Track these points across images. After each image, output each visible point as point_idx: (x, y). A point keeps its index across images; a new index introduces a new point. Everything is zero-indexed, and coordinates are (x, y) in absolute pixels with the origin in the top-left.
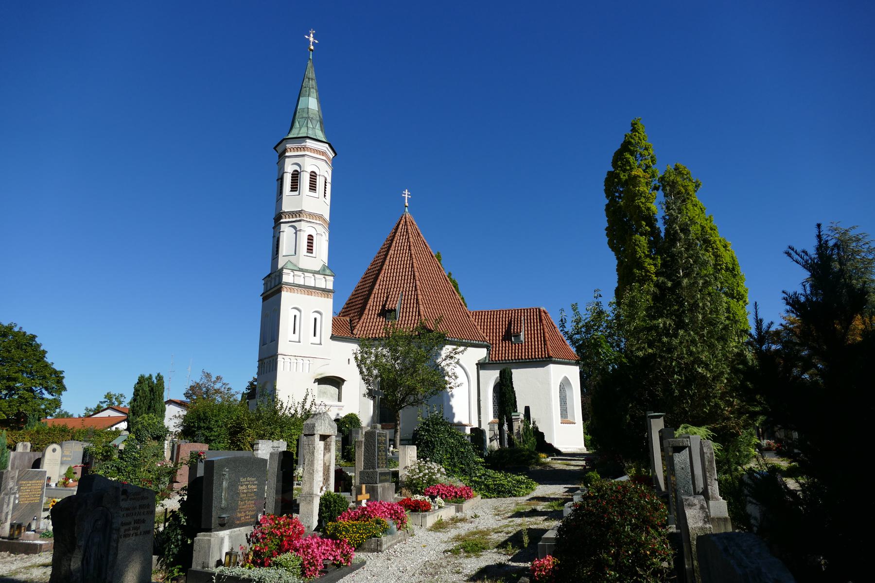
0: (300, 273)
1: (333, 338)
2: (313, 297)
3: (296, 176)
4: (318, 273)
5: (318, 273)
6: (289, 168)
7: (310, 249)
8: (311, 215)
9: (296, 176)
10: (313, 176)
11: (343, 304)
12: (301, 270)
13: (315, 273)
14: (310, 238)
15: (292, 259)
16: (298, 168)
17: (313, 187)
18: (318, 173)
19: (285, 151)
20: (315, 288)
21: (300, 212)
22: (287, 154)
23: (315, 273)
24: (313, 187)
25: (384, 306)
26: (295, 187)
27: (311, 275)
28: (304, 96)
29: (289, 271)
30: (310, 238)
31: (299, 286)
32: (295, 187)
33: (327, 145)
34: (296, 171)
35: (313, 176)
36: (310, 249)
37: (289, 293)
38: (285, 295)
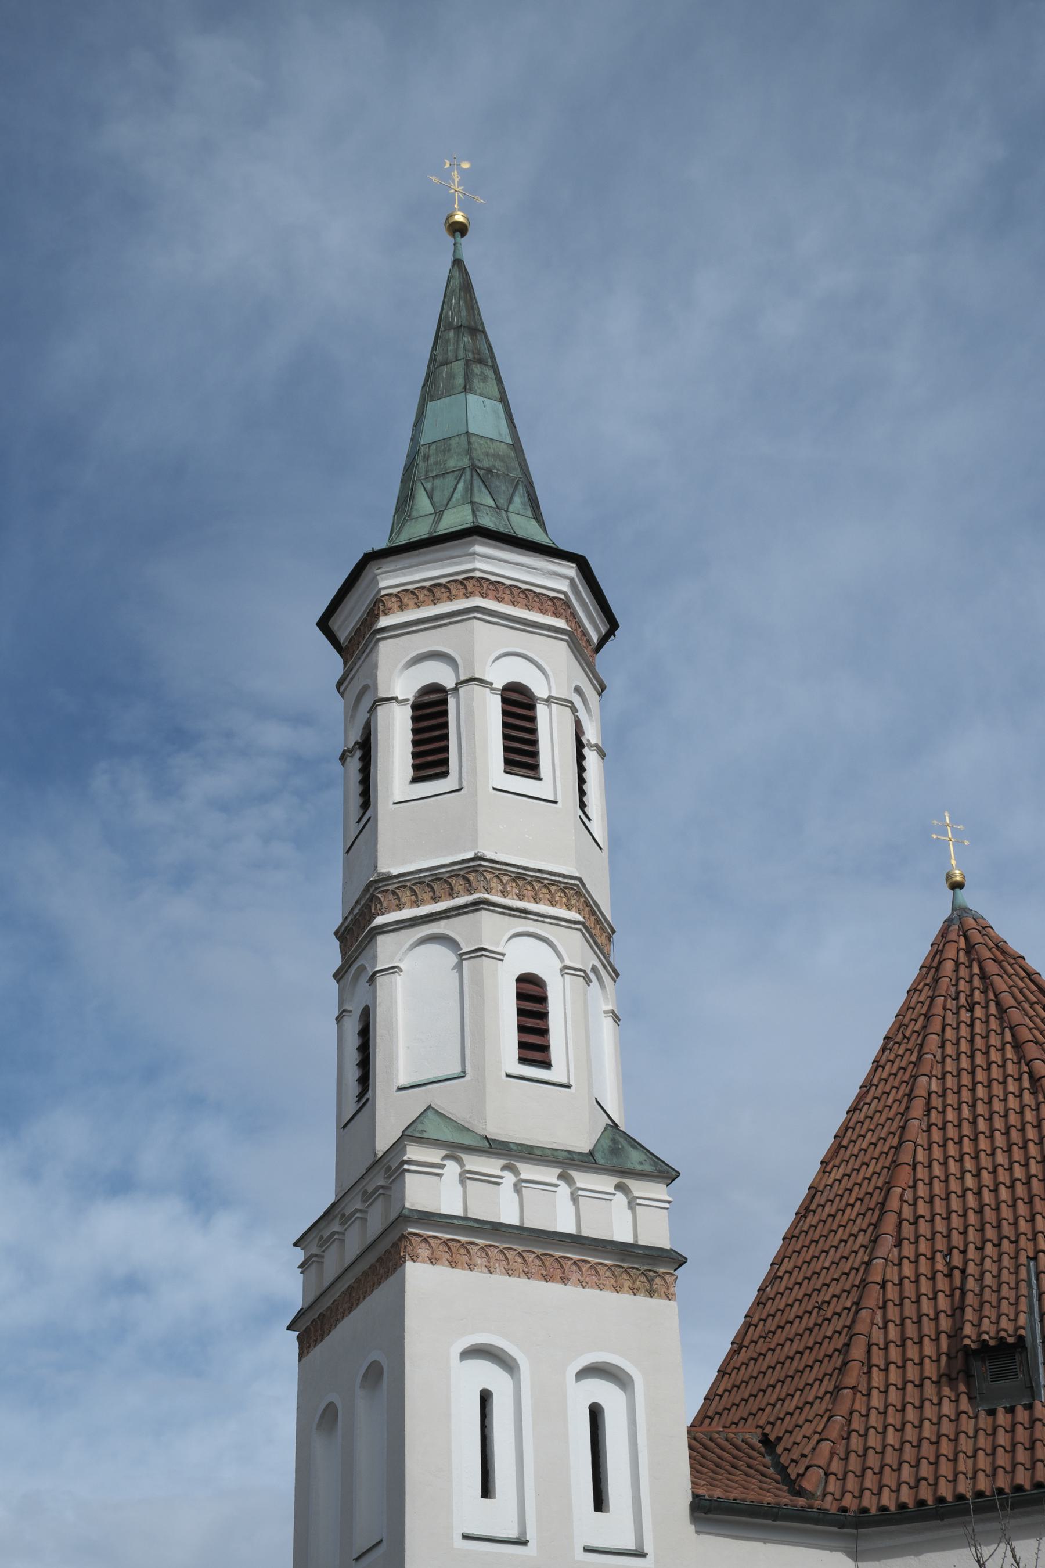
0: (491, 1166)
1: (707, 1511)
2: (478, 1278)
3: (431, 713)
4: (587, 1161)
5: (587, 1161)
6: (399, 676)
7: (534, 1047)
8: (527, 880)
9: (431, 713)
10: (518, 705)
11: (398, 1271)
12: (494, 1147)
13: (568, 1162)
14: (531, 995)
15: (441, 1098)
16: (442, 675)
17: (521, 754)
18: (539, 689)
19: (377, 607)
20: (576, 1241)
21: (474, 871)
22: (384, 622)
23: (568, 1162)
24: (521, 754)
25: (956, 1334)
26: (431, 757)
27: (549, 1174)
28: (449, 392)
29: (434, 1155)
30: (531, 995)
31: (496, 1229)
32: (431, 757)
33: (570, 570)
34: (435, 689)
35: (518, 705)
36: (534, 1047)
37: (442, 1271)
38: (426, 1283)
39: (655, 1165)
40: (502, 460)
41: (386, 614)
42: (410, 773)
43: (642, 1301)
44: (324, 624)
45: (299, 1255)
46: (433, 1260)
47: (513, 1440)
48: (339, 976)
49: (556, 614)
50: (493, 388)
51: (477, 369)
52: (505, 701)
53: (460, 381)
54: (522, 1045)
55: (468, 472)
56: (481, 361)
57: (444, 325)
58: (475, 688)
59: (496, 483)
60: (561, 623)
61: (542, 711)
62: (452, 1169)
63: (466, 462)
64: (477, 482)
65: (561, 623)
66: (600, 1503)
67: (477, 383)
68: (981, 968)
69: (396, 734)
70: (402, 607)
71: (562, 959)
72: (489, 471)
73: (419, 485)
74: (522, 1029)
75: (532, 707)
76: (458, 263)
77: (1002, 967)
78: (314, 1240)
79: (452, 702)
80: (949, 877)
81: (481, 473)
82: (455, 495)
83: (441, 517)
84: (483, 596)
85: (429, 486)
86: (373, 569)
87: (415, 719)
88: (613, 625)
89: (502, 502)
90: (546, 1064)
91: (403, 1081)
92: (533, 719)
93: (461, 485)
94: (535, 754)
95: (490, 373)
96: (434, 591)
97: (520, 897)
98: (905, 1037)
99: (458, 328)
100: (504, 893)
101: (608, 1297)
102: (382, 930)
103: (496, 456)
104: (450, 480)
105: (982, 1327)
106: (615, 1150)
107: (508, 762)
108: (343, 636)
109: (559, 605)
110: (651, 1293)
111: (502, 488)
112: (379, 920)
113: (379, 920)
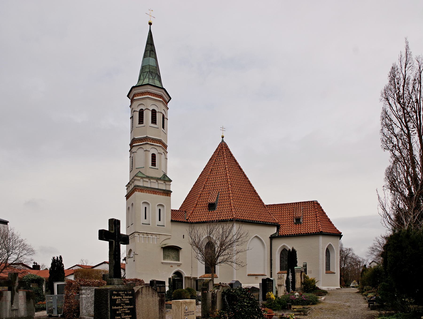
7: (154, 164)
10: (154, 112)
12: (148, 177)
13: (158, 179)
14: (154, 156)
15: (141, 170)
17: (154, 121)
20: (158, 189)
24: (154, 121)
30: (154, 156)
34: (142, 109)
35: (154, 112)
36: (154, 164)
42: (138, 123)
43: (166, 197)
44: (128, 96)
45: (126, 188)
46: (139, 191)
48: (130, 151)
49: (160, 98)
50: (154, 56)
51: (152, 52)
53: (149, 55)
54: (152, 163)
56: (152, 51)
57: (147, 43)
58: (147, 110)
60: (161, 100)
62: (141, 180)
64: (150, 74)
65: (161, 100)
66: (160, 220)
67: (151, 55)
70: (138, 96)
74: (152, 161)
75: (156, 113)
76: (150, 31)
78: (128, 186)
84: (149, 95)
86: (133, 90)
88: (171, 98)
89: (154, 78)
90: (155, 166)
91: (137, 167)
92: (156, 115)
94: (156, 121)
95: (153, 53)
96: (142, 94)
97: (153, 142)
100: (150, 142)
101: (162, 196)
102: (134, 146)
103: (153, 69)
104: (146, 73)
106: (164, 178)
109: (161, 96)
110: (167, 196)
111: (154, 75)
112: (134, 145)
113: (134, 145)
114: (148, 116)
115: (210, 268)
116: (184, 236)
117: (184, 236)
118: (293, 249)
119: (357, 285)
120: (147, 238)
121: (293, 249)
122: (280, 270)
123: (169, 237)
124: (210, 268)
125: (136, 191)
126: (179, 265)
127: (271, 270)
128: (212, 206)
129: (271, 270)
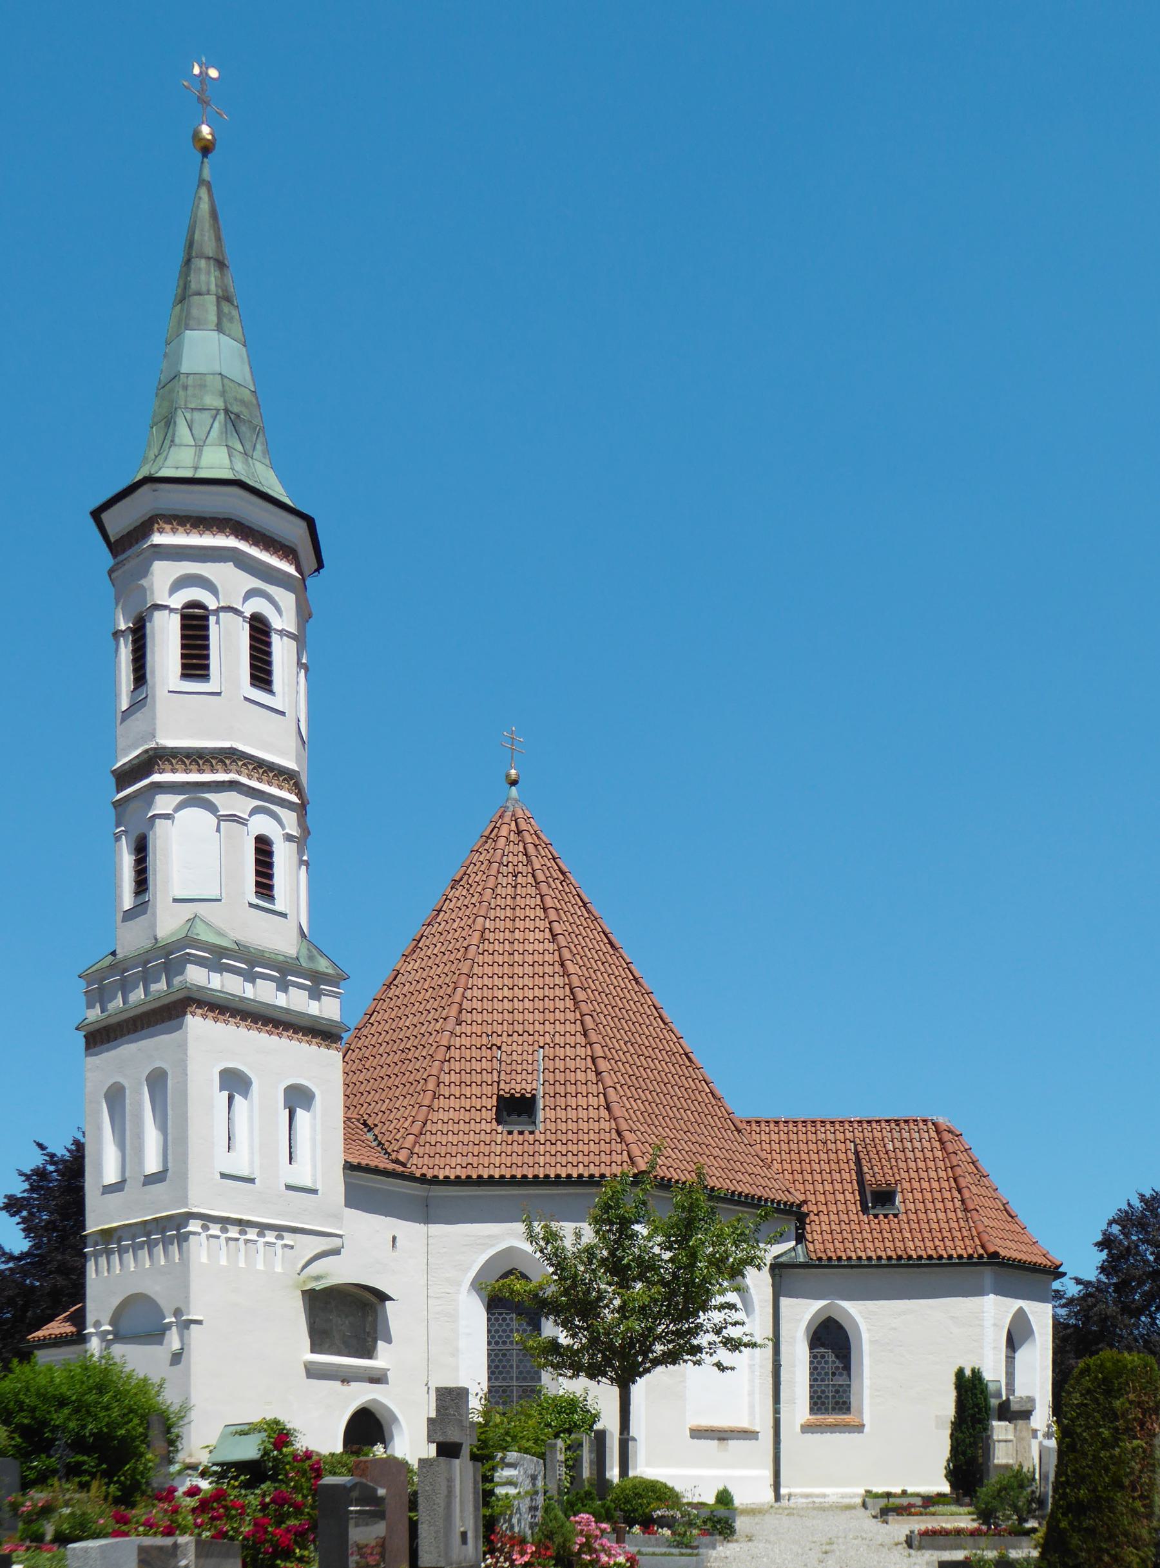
3: (195, 627)
10: (260, 630)
22: (158, 539)
26: (195, 663)
32: (195, 663)
33: (303, 524)
39: (334, 969)
40: (247, 407)
41: (161, 533)
46: (204, 1016)
47: (770, 1380)
51: (226, 308)
52: (252, 627)
53: (213, 318)
55: (222, 413)
59: (243, 429)
61: (275, 639)
63: (219, 403)
67: (226, 324)
68: (525, 848)
69: (167, 637)
71: (283, 827)
72: (238, 416)
73: (179, 412)
77: (537, 850)
79: (212, 619)
80: (508, 776)
81: (233, 416)
82: (212, 433)
83: (201, 451)
85: (188, 416)
87: (184, 627)
88: (320, 565)
89: (248, 446)
93: (216, 425)
98: (817, 1215)
99: (209, 258)
103: (243, 402)
105: (517, 1086)
107: (253, 676)
108: (114, 532)
114: (229, 644)
115: (1028, 1275)
116: (394, 1238)
117: (394, 1238)
118: (6, 1196)
119: (1011, 1437)
120: (241, 1242)
121: (6, 1196)
122: (812, 1411)
123: (334, 1243)
124: (1028, 1275)
125: (193, 1014)
126: (378, 1378)
127: (777, 1411)
128: (516, 1109)
129: (777, 1411)
